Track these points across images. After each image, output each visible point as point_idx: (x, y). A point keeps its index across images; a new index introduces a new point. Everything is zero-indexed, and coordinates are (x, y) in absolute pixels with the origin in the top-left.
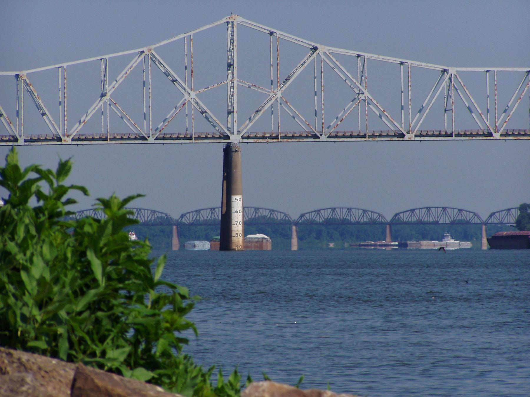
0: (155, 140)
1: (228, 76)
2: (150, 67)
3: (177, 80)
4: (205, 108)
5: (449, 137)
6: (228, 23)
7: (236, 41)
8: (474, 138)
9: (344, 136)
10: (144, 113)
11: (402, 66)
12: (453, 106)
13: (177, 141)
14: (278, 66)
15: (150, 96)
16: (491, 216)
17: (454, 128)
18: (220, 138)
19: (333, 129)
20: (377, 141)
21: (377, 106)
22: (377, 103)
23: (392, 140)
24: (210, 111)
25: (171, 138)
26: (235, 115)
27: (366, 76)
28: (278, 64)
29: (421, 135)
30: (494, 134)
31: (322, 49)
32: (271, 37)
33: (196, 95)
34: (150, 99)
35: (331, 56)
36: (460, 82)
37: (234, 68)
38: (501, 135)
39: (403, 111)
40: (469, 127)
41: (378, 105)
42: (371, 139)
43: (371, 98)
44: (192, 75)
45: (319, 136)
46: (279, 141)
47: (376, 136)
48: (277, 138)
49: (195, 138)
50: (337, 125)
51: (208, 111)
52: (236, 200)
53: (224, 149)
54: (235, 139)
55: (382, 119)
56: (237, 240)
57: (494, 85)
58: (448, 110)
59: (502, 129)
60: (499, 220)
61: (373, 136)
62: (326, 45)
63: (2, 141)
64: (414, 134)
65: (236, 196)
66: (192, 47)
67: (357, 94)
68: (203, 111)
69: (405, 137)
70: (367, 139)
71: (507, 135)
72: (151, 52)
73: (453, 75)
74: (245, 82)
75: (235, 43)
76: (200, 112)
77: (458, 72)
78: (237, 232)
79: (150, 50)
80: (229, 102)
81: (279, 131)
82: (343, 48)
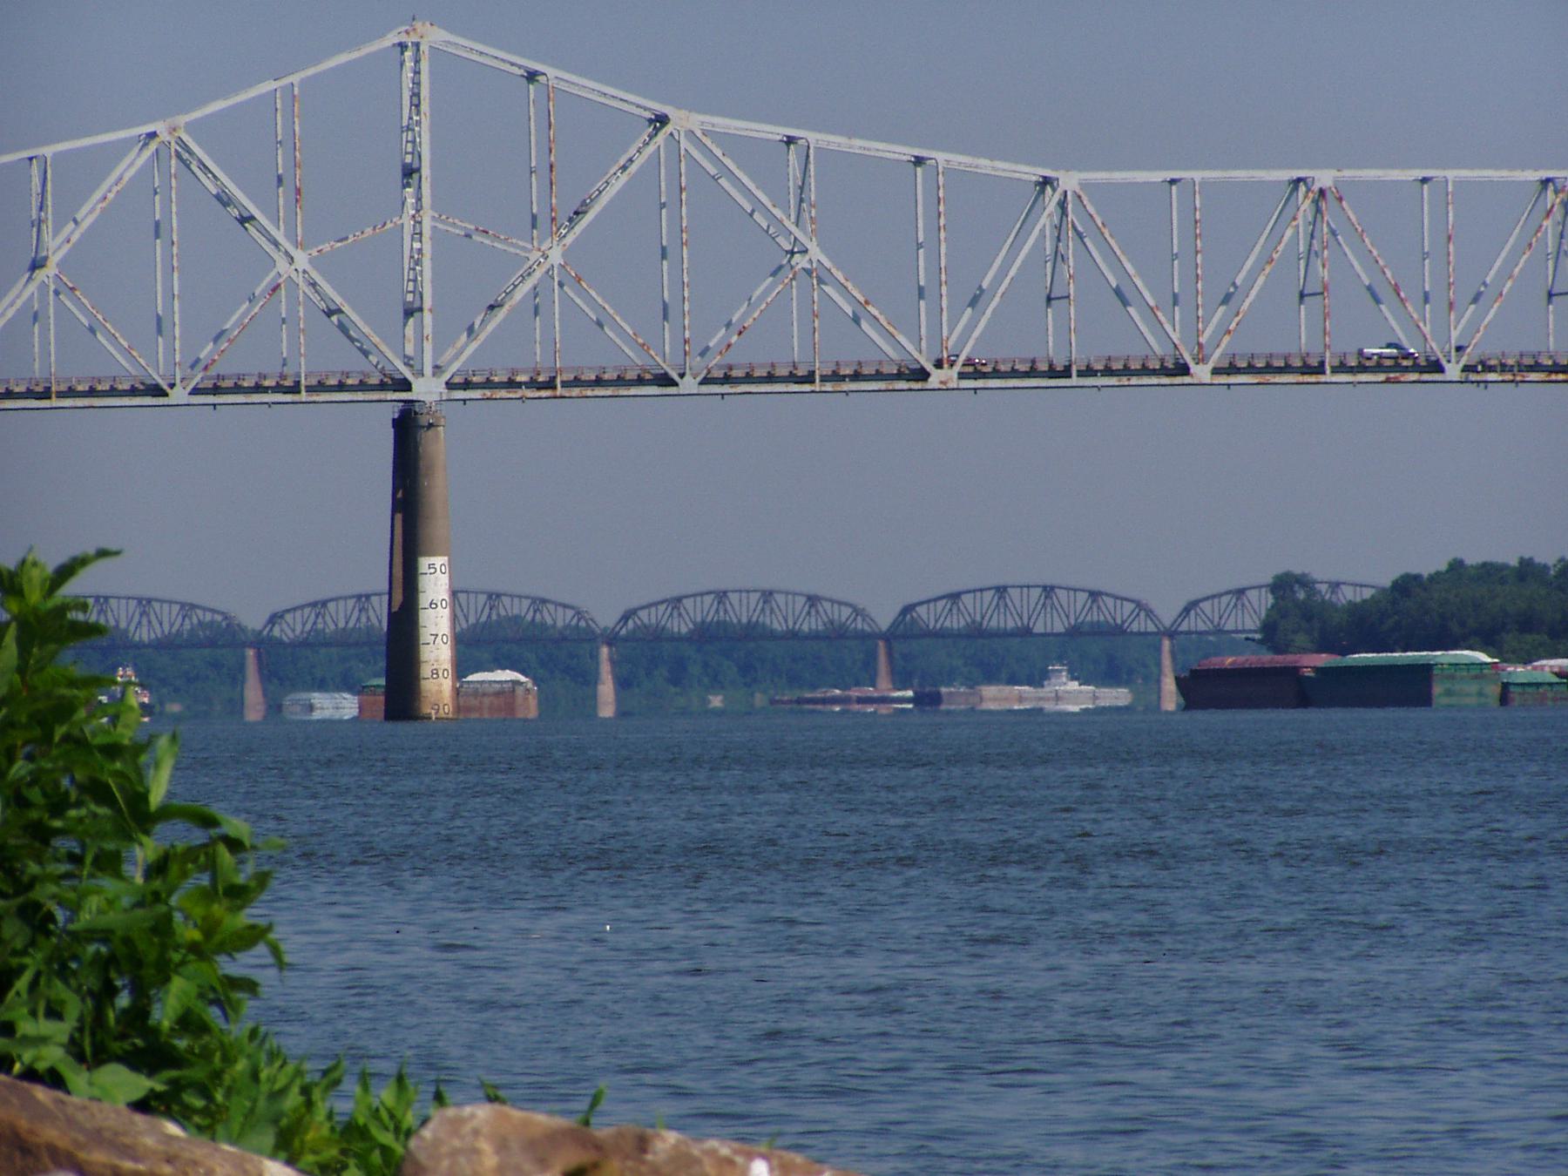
0: (190, 394)
1: (403, 204)
3: (251, 218)
4: (338, 300)
6: (403, 47)
7: (427, 101)
8: (1134, 381)
9: (749, 378)
11: (919, 169)
12: (1071, 285)
13: (256, 398)
14: (551, 171)
16: (1187, 610)
23: (891, 388)
24: (354, 308)
25: (237, 389)
26: (427, 317)
27: (813, 199)
28: (551, 166)
31: (682, 120)
32: (531, 86)
35: (707, 142)
36: (1091, 216)
38: (1216, 371)
41: (850, 286)
42: (828, 387)
43: (827, 263)
45: (676, 378)
47: (843, 378)
48: (551, 385)
49: (310, 389)
50: (729, 346)
51: (346, 309)
53: (394, 420)
54: (427, 390)
61: (836, 377)
65: (432, 560)
66: (296, 120)
67: (787, 252)
69: (930, 379)
71: (1232, 369)
73: (1069, 194)
74: (456, 221)
75: (425, 107)
77: (1084, 185)
78: (435, 667)
79: (174, 130)
81: (558, 366)
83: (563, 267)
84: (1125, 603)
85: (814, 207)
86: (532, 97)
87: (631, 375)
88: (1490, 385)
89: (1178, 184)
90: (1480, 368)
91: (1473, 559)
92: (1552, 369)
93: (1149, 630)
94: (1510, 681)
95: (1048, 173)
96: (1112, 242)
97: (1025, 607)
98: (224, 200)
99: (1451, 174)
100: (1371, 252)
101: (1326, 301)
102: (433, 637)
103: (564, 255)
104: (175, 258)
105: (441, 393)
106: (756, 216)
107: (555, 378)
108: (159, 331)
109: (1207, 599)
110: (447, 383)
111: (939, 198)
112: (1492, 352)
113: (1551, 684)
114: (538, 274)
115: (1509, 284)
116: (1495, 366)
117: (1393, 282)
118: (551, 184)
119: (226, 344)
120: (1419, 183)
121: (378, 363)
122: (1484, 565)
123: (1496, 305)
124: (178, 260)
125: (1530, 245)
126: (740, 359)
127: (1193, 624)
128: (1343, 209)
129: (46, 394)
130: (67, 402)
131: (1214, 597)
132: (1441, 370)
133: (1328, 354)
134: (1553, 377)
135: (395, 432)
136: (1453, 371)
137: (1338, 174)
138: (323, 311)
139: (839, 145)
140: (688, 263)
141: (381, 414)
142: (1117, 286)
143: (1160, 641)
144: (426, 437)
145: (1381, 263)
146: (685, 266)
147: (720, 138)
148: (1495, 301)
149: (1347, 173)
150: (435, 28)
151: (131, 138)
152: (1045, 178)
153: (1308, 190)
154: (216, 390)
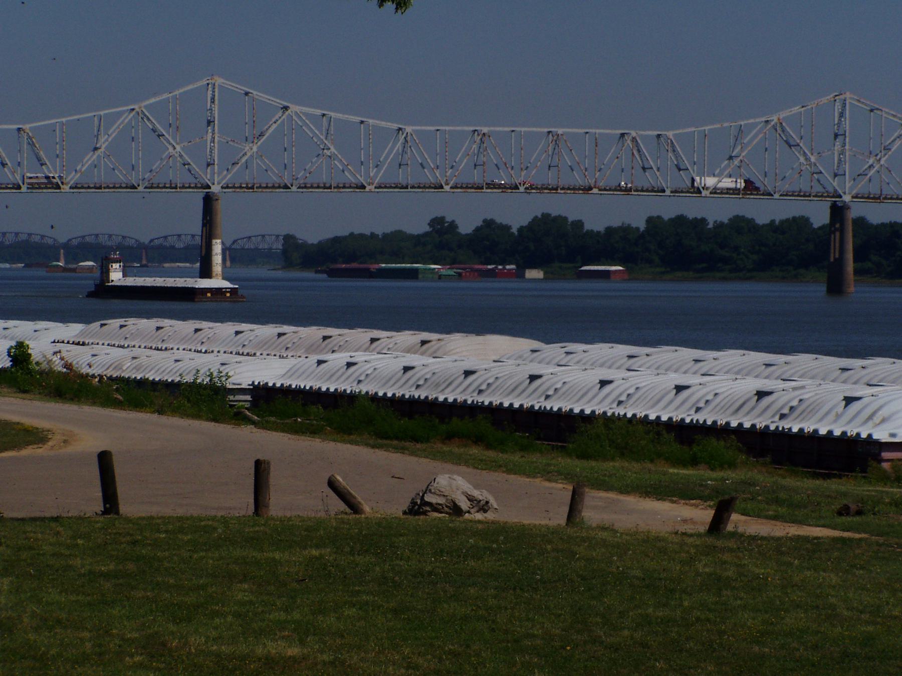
3: (164, 135)
4: (189, 161)
6: (208, 84)
8: (427, 190)
9: (312, 187)
13: (164, 190)
20: (416, 192)
25: (158, 187)
26: (216, 167)
29: (380, 187)
31: (294, 108)
33: (182, 149)
35: (301, 115)
40: (423, 180)
42: (336, 190)
43: (336, 153)
47: (340, 188)
50: (306, 177)
51: (191, 163)
54: (215, 189)
70: (332, 190)
75: (216, 102)
77: (413, 130)
87: (124, 185)
91: (356, 232)
95: (21, 126)
98: (154, 130)
103: (257, 148)
106: (314, 138)
108: (133, 169)
114: (249, 154)
126: (309, 181)
129: (100, 188)
130: (107, 190)
141: (199, 195)
147: (304, 114)
153: (478, 135)
154: (151, 187)
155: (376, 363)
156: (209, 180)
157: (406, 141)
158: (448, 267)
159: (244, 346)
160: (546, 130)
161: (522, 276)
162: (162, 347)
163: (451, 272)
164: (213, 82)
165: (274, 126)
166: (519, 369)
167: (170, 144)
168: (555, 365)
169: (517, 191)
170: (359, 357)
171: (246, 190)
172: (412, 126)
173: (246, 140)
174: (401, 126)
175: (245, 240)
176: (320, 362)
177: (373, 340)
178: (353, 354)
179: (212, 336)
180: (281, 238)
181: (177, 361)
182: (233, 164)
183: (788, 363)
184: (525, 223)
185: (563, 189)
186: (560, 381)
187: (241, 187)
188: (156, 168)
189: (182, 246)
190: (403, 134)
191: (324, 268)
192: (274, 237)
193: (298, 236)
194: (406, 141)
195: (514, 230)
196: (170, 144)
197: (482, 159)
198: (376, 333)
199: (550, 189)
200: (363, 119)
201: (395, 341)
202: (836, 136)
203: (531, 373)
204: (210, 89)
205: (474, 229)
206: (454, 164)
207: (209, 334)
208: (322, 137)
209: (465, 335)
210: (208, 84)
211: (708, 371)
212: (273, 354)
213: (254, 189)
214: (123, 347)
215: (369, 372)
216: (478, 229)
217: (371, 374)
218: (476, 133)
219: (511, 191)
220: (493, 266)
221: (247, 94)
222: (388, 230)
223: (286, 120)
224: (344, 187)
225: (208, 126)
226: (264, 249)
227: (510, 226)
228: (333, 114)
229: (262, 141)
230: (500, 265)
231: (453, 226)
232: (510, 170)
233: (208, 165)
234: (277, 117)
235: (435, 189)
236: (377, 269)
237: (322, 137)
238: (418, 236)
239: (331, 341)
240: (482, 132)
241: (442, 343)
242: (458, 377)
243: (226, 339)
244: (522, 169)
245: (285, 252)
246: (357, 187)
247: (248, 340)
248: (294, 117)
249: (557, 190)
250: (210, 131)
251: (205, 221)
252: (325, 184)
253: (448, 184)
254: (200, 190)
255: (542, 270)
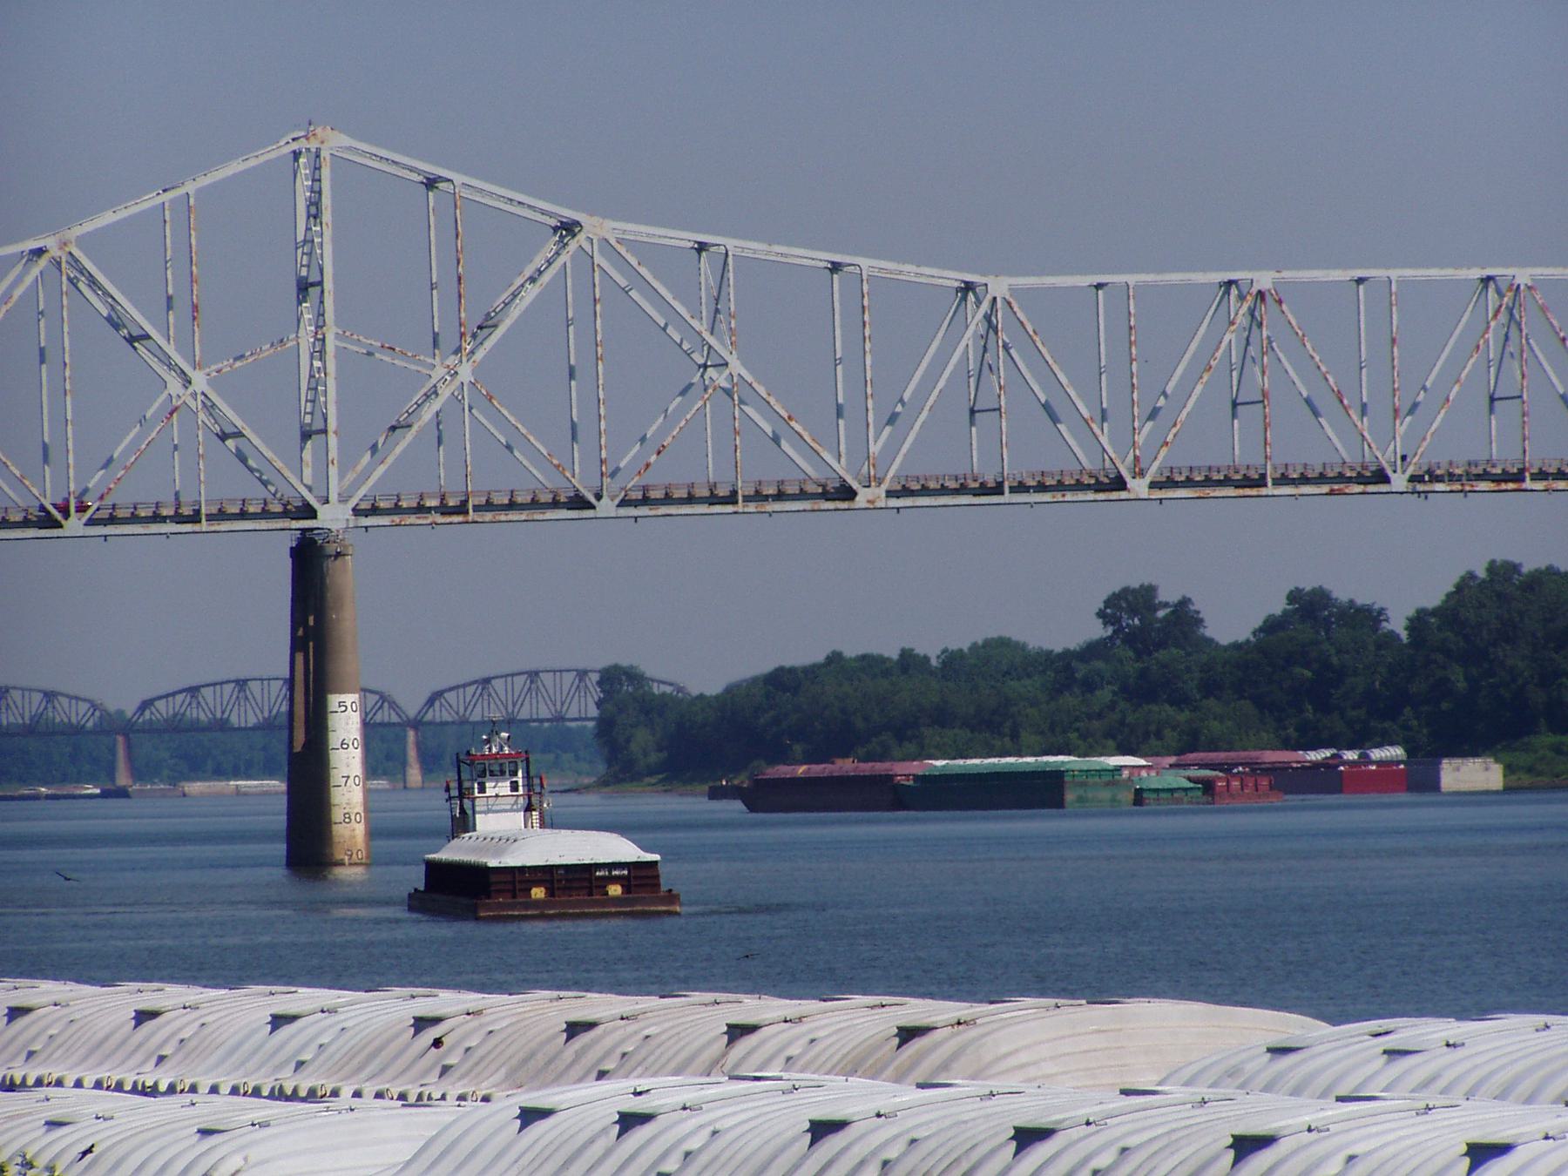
0: (85, 525)
1: (299, 321)
2: (64, 297)
3: (147, 337)
4: (239, 423)
5: (982, 497)
6: (296, 155)
7: (329, 209)
8: (1069, 497)
9: (668, 500)
10: (43, 442)
11: (835, 276)
12: (1002, 397)
13: (154, 528)
14: (460, 283)
15: (68, 387)
16: (431, 702)
17: (1006, 467)
18: (285, 514)
19: (636, 479)
20: (1031, 505)
21: (768, 403)
22: (769, 395)
23: (816, 507)
24: (255, 431)
25: (134, 519)
26: (333, 440)
27: (732, 309)
28: (459, 279)
29: (906, 492)
30: (1131, 483)
31: (595, 227)
32: (430, 193)
33: (211, 382)
34: (68, 398)
35: (622, 250)
36: (1022, 323)
37: (326, 294)
38: (1154, 485)
39: (841, 422)
40: (1053, 464)
41: (772, 401)
42: (752, 507)
43: (749, 378)
44: (194, 318)
45: (593, 500)
46: (470, 519)
47: (766, 498)
48: (461, 509)
49: (210, 518)
50: (648, 465)
51: (247, 432)
52: (344, 708)
53: (292, 548)
54: (332, 518)
55: (780, 447)
56: (347, 833)
57: (1127, 329)
58: (979, 411)
59: (1156, 464)
60: (457, 713)
61: (758, 497)
62: (607, 214)
63: (4, 524)
64: (885, 487)
65: (342, 697)
66: (192, 232)
67: (700, 366)
68: (226, 431)
69: (857, 498)
70: (740, 507)
71: (1170, 483)
72: (67, 249)
73: (999, 300)
74: (361, 338)
75: (327, 216)
76: (217, 434)
77: (1013, 290)
78: (346, 811)
79: (65, 244)
80: (307, 401)
81: (469, 489)
82: (647, 223)
83: (474, 384)
84: (367, 694)
85: (734, 317)
86: (431, 205)
88: (1429, 495)
89: (1105, 288)
90: (1427, 478)
91: (851, 651)
92: (1502, 477)
93: (392, 721)
94: (1144, 787)
96: (1044, 350)
97: (266, 699)
99: (1394, 274)
100: (1312, 357)
101: (1267, 410)
102: (345, 779)
103: (473, 373)
104: (68, 381)
105: (348, 520)
106: (670, 330)
107: (466, 501)
109: (451, 689)
110: (354, 510)
111: (863, 307)
112: (1442, 463)
113: (1186, 790)
114: (445, 393)
115: (1456, 388)
116: (1442, 476)
117: (1336, 389)
118: (460, 296)
119: (123, 472)
120: (1354, 284)
121: (276, 491)
122: (864, 657)
123: (1443, 411)
124: (71, 383)
125: (1478, 347)
126: (658, 480)
127: (438, 714)
128: (1283, 312)
131: (457, 687)
132: (1386, 480)
133: (1269, 467)
134: (1503, 486)
135: (293, 564)
136: (1399, 481)
137: (1277, 275)
138: (217, 434)
139: (755, 251)
140: (604, 378)
141: (279, 540)
142: (1046, 401)
143: (405, 731)
144: (332, 566)
145: (1323, 369)
146: (601, 382)
147: (633, 245)
148: (1442, 408)
149: (1287, 274)
150: (335, 132)
151: (13, 255)
152: (966, 283)
153: (1242, 298)
155: (720, 1113)
156: (310, 489)
157: (992, 327)
158: (1173, 760)
159: (300, 1064)
160: (1477, 273)
161: (1433, 785)
162: (24, 1079)
163: (1177, 780)
164: (313, 145)
165: (531, 292)
166: (1201, 1115)
167: (171, 366)
168: (1555, 1101)
169: (1383, 488)
170: (664, 1093)
171: (440, 519)
172: (1011, 274)
173: (435, 344)
174: (969, 278)
175: (179, 698)
176: (529, 1116)
177: (737, 1032)
178: (643, 1084)
179: (195, 1034)
180: (595, 677)
181: (53, 1124)
182: (393, 428)
183: (1454, 1046)
184: (1433, 599)
185: (1541, 475)
186: (1339, 1149)
187: (421, 509)
188: (125, 453)
189: (252, 721)
190: (979, 303)
191: (742, 780)
192: (569, 678)
193: (649, 669)
194: (992, 327)
195: (1397, 624)
196: (171, 366)
197: (1258, 380)
198: (749, 1008)
199: (1497, 479)
200: (837, 258)
201: (810, 1031)
202: (304, 287)
203: (1237, 1132)
204: (304, 171)
205: (1258, 623)
206: (1162, 402)
207: (180, 1029)
208: (701, 326)
209: (1052, 1001)
210: (296, 155)
211: (1356, 1089)
212: (395, 1092)
213: (735, 503)
214: (151, 1092)
215: (694, 1144)
216: (1272, 626)
217: (701, 1150)
218: (1234, 291)
219: (1359, 488)
220: (1328, 753)
221: (431, 183)
222: (961, 641)
223: (568, 265)
224: (780, 496)
225: (300, 303)
226: (541, 721)
227: (1381, 611)
228: (731, 243)
229: (489, 344)
230: (1349, 748)
231: (1184, 618)
232: (1355, 417)
233: (306, 435)
234: (539, 261)
235: (1097, 491)
236: (916, 778)
237: (701, 326)
238: (1067, 654)
239: (595, 1042)
240: (1254, 290)
241: (973, 1033)
242: (993, 1152)
243: (240, 1044)
244: (1396, 411)
245: (606, 726)
246: (826, 495)
247: (315, 1046)
248: (598, 259)
249: (1523, 480)
250: (307, 316)
251: (300, 633)
252: (712, 487)
253: (1142, 474)
254: (279, 524)
255: (1497, 761)
